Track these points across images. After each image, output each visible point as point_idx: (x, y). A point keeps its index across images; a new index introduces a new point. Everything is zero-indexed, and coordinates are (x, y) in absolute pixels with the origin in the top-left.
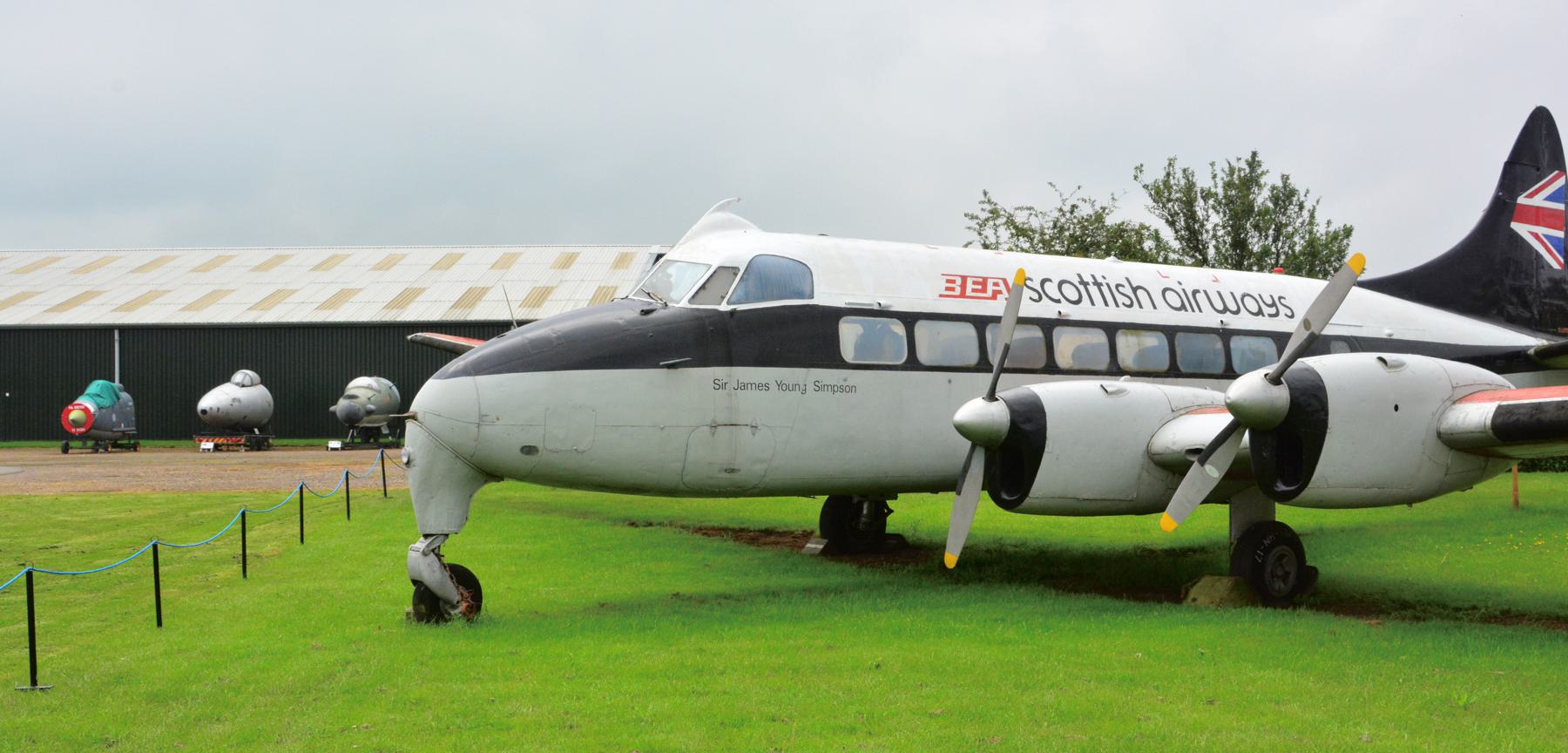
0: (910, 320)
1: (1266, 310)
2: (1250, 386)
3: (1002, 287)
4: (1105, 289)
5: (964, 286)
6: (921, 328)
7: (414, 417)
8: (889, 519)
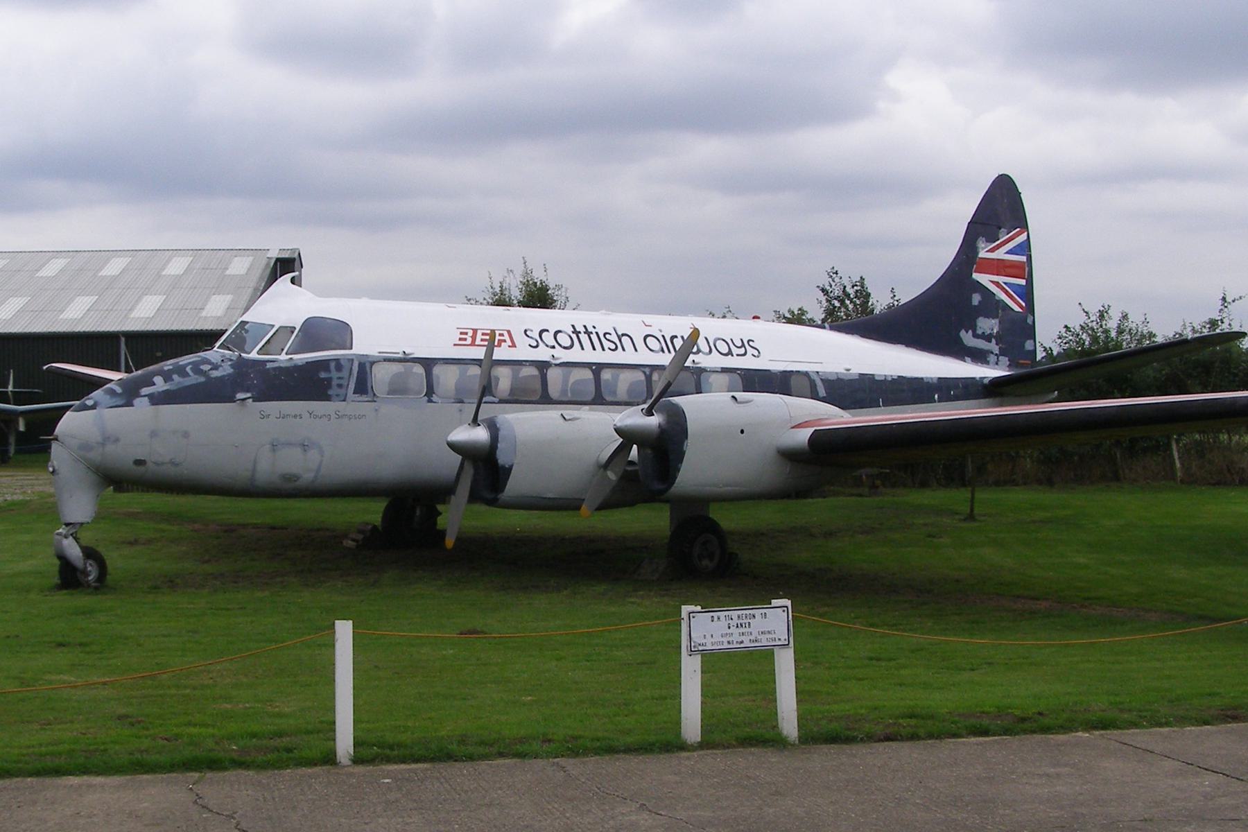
0: (428, 364)
1: (735, 351)
2: (634, 418)
3: (506, 337)
4: (594, 337)
5: (474, 338)
6: (437, 370)
7: (56, 439)
8: (439, 518)
